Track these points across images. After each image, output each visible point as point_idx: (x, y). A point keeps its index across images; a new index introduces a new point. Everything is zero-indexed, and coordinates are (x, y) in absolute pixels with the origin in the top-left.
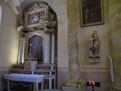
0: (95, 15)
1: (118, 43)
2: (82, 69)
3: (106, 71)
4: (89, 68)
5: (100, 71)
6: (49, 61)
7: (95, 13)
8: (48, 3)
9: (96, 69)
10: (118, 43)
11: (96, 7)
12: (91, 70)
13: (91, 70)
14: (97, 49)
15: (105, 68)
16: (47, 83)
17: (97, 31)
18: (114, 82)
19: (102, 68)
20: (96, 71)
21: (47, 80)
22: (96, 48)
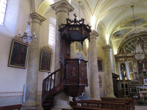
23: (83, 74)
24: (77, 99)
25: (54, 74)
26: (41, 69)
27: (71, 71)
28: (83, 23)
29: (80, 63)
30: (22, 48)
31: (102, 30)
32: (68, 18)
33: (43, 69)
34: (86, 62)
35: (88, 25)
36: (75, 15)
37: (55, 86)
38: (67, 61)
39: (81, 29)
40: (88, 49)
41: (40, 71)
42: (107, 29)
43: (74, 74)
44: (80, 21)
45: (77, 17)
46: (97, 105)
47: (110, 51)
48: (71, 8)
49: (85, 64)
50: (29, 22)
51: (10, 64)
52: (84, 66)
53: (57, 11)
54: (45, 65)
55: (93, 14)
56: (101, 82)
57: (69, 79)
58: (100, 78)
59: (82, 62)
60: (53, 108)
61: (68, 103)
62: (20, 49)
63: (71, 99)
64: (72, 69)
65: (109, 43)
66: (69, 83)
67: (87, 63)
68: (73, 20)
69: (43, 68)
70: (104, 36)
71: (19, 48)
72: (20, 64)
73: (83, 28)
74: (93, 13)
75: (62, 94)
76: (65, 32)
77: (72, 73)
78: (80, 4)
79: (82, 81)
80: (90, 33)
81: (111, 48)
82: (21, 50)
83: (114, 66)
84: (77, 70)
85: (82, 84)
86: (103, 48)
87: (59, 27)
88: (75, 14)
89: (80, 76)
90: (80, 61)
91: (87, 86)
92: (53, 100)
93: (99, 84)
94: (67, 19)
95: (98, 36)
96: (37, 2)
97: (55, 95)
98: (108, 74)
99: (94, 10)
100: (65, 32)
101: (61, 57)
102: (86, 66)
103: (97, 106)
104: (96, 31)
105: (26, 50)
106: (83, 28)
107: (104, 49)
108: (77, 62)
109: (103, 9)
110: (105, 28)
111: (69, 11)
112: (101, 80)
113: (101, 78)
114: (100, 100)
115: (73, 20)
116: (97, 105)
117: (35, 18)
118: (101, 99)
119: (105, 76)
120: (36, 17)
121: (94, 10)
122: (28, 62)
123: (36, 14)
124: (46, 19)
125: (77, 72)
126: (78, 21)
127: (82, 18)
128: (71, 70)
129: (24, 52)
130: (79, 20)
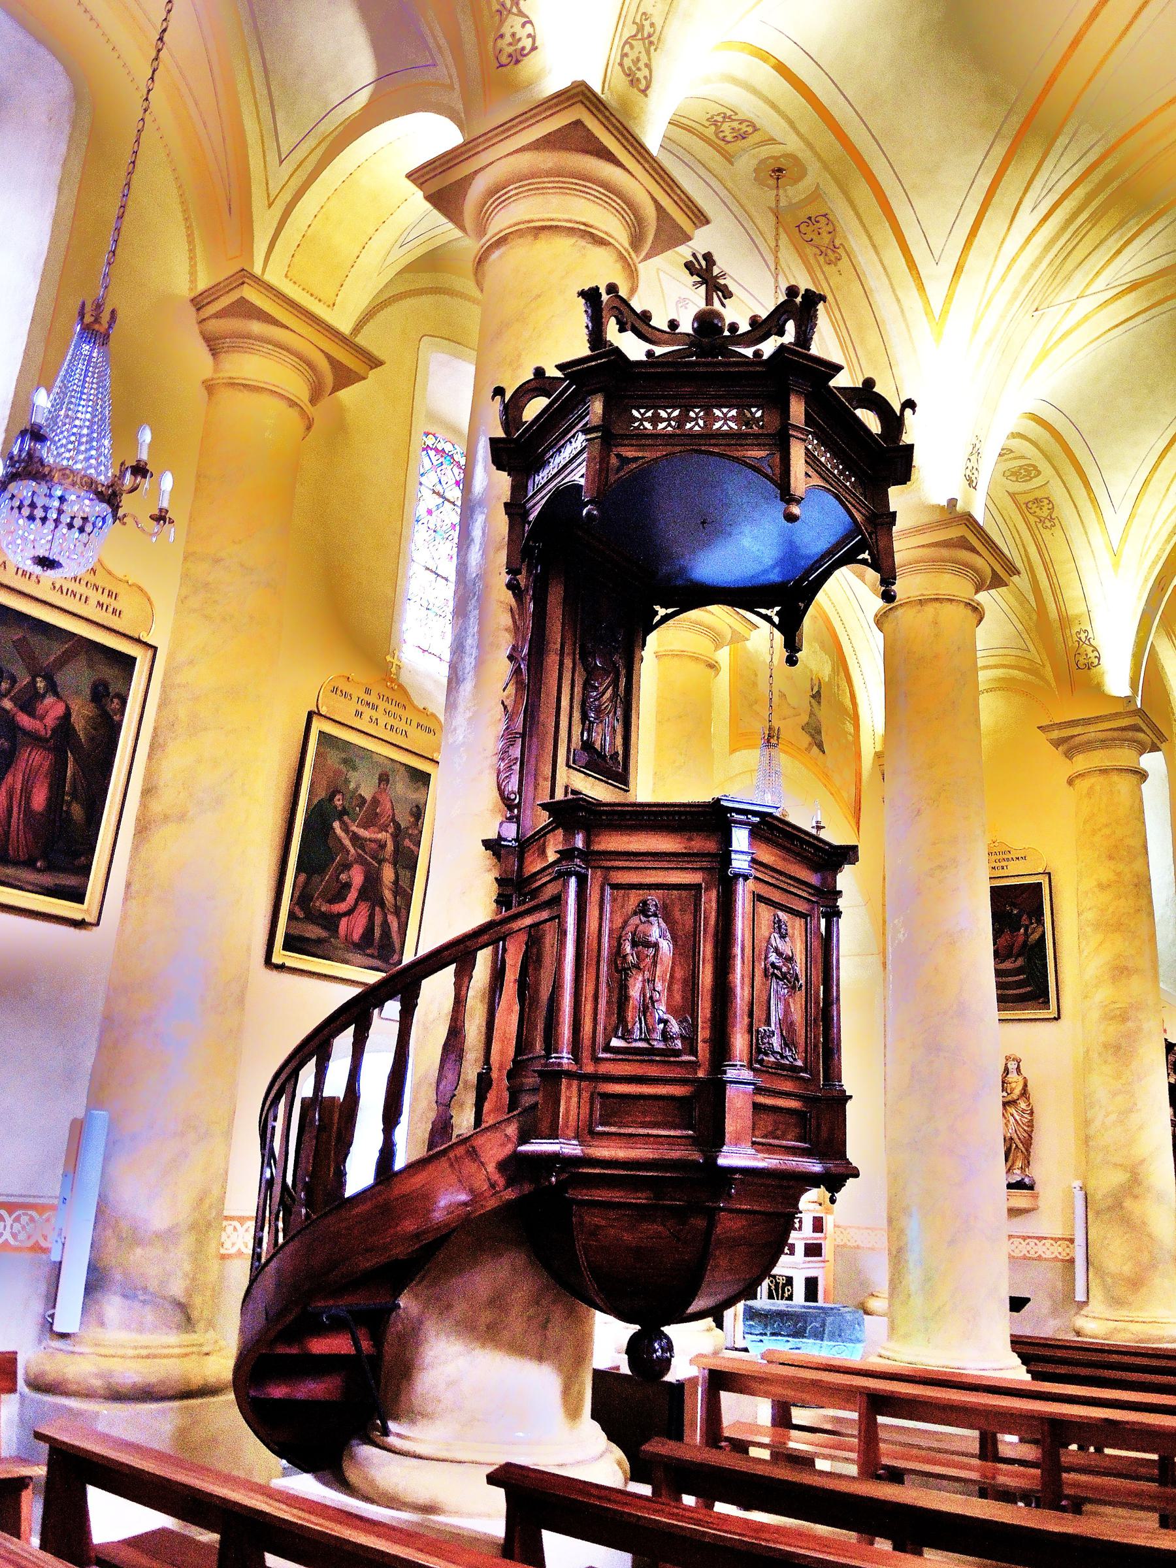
0: (1018, 971)
1: (1103, 1123)
2: (17, 1219)
3: (1060, 1249)
4: (1018, 1237)
5: (17, 1219)
6: (483, 1029)
7: (1020, 962)
8: (639, 289)
9: (1048, 1245)
10: (1103, 1123)
11: (1022, 930)
12: (1029, 1248)
13: (1029, 1248)
14: (1021, 1146)
15: (1060, 1239)
16: (783, 1292)
17: (1019, 1056)
18: (1084, 1299)
19: (1046, 1238)
20: (1048, 1253)
21: (781, 1281)
22: (1011, 1139)
23: (787, 1025)
24: (692, 1347)
25: (393, 1008)
26: (287, 947)
27: (621, 971)
28: (804, 338)
29: (740, 863)
30: (59, 678)
31: (1051, 520)
32: (612, 288)
33: (320, 941)
34: (836, 867)
35: (867, 394)
36: (704, 272)
37: (399, 1163)
38: (566, 843)
39: (774, 424)
40: (878, 756)
41: (281, 968)
42: (1115, 520)
43: (661, 1010)
44: (761, 328)
45: (727, 294)
46: (967, 1437)
47: (1142, 775)
48: (666, 202)
49: (817, 891)
50: (99, 307)
51: (287, 947)
52: (802, 907)
53: (490, 233)
54: (340, 896)
55: (945, 311)
56: (1028, 1143)
57: (589, 1068)
58: (1017, 1097)
59: (767, 855)
60: (428, 1393)
61: (566, 1391)
62: (41, 684)
63: (609, 1339)
64: (641, 942)
65: (1134, 685)
66: (587, 1133)
67: (845, 879)
68: (673, 324)
69: (313, 931)
70: (1071, 593)
71: (24, 680)
72: (29, 864)
73: (797, 410)
74: (949, 298)
75: (497, 1275)
76: (571, 462)
77: (635, 992)
78: (794, 193)
79: (757, 1107)
80: (893, 491)
81: (1154, 748)
82: (50, 700)
83: (332, 1530)
84: (706, 949)
85: (770, 1149)
86: (1057, 743)
87: (506, 408)
88: (708, 257)
89: (740, 1042)
90: (740, 838)
91: (834, 1182)
92: (378, 1339)
93: (998, 1173)
94: (591, 296)
95: (997, 582)
96: (273, 158)
97: (401, 1274)
98: (1120, 1050)
99: (959, 269)
100: (571, 462)
101: (513, 785)
102: (833, 914)
103: (975, 1447)
104: (979, 516)
105: (107, 705)
106: (797, 410)
107: (1069, 754)
108: (706, 844)
109: (1063, 261)
110: (1094, 500)
111: (636, 241)
112: (1031, 1124)
113: (1025, 1093)
114: (1016, 1373)
115: (673, 324)
116: (967, 1437)
117: (248, 336)
118: (1026, 1359)
119: (1085, 1068)
120: (256, 327)
121: (959, 269)
122: (136, 848)
123: (250, 294)
124: (375, 363)
125: (706, 977)
126: (744, 327)
127: (792, 291)
128: (617, 952)
129: (79, 723)
130: (754, 321)
